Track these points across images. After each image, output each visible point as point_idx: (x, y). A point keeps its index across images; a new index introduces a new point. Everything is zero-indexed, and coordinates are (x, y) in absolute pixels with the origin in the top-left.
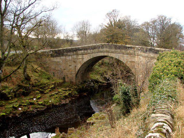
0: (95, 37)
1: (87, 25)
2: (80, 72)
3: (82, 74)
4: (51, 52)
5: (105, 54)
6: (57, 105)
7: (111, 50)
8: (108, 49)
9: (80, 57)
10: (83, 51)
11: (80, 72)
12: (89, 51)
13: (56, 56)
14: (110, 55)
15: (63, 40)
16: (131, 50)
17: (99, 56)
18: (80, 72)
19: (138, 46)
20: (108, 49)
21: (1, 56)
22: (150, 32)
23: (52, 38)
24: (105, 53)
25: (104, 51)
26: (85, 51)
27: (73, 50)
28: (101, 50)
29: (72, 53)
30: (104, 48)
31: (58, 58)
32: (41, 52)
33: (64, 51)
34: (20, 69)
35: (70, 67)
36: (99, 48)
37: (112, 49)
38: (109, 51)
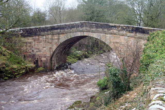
9: (56, 38)
10: (59, 31)
20: (88, 29)
25: (83, 30)
26: (62, 31)
30: (83, 26)
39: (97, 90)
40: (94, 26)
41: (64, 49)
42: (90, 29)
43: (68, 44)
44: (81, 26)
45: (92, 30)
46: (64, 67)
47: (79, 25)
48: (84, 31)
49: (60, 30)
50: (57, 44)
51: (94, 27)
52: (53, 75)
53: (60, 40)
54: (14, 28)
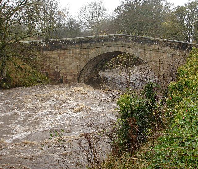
0: (112, 26)
1: (100, 9)
2: (84, 73)
3: (87, 75)
4: (44, 43)
5: (120, 49)
7: (128, 44)
10: (89, 44)
13: (50, 50)
14: (127, 50)
15: (65, 29)
16: (156, 45)
18: (85, 73)
19: (167, 40)
20: (124, 43)
22: (185, 22)
24: (120, 48)
26: (92, 44)
27: (75, 42)
29: (73, 46)
30: (118, 40)
31: (55, 52)
32: (30, 43)
34: (90, 54)
36: (112, 40)
37: (129, 42)
38: (126, 45)
44: (115, 40)
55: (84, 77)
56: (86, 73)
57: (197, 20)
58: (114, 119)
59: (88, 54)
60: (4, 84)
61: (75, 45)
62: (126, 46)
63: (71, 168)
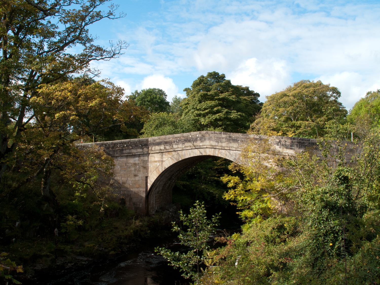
2: (155, 188)
3: (158, 192)
6: (8, 269)
7: (220, 144)
8: (214, 143)
9: (157, 159)
10: (162, 147)
11: (156, 189)
12: (175, 146)
17: (187, 157)
18: (156, 189)
20: (214, 143)
21: (236, 282)
23: (18, 145)
24: (207, 150)
25: (205, 145)
26: (168, 147)
28: (199, 143)
30: (205, 140)
33: (124, 147)
35: (137, 178)
37: (221, 142)
38: (216, 146)
39: (309, 269)
40: (223, 138)
41: (169, 180)
42: (217, 144)
43: (177, 172)
44: (200, 140)
45: (222, 146)
46: (168, 210)
47: (198, 137)
48: (205, 147)
49: (164, 146)
50: (159, 170)
51: (224, 140)
52: (377, 256)
53: (164, 163)
54: (122, 141)
55: (154, 195)
56: (157, 190)
57: (379, 273)
58: (152, 281)
59: (162, 161)
60: (46, 205)
61: (143, 149)
62: (217, 147)
63: (312, 284)
